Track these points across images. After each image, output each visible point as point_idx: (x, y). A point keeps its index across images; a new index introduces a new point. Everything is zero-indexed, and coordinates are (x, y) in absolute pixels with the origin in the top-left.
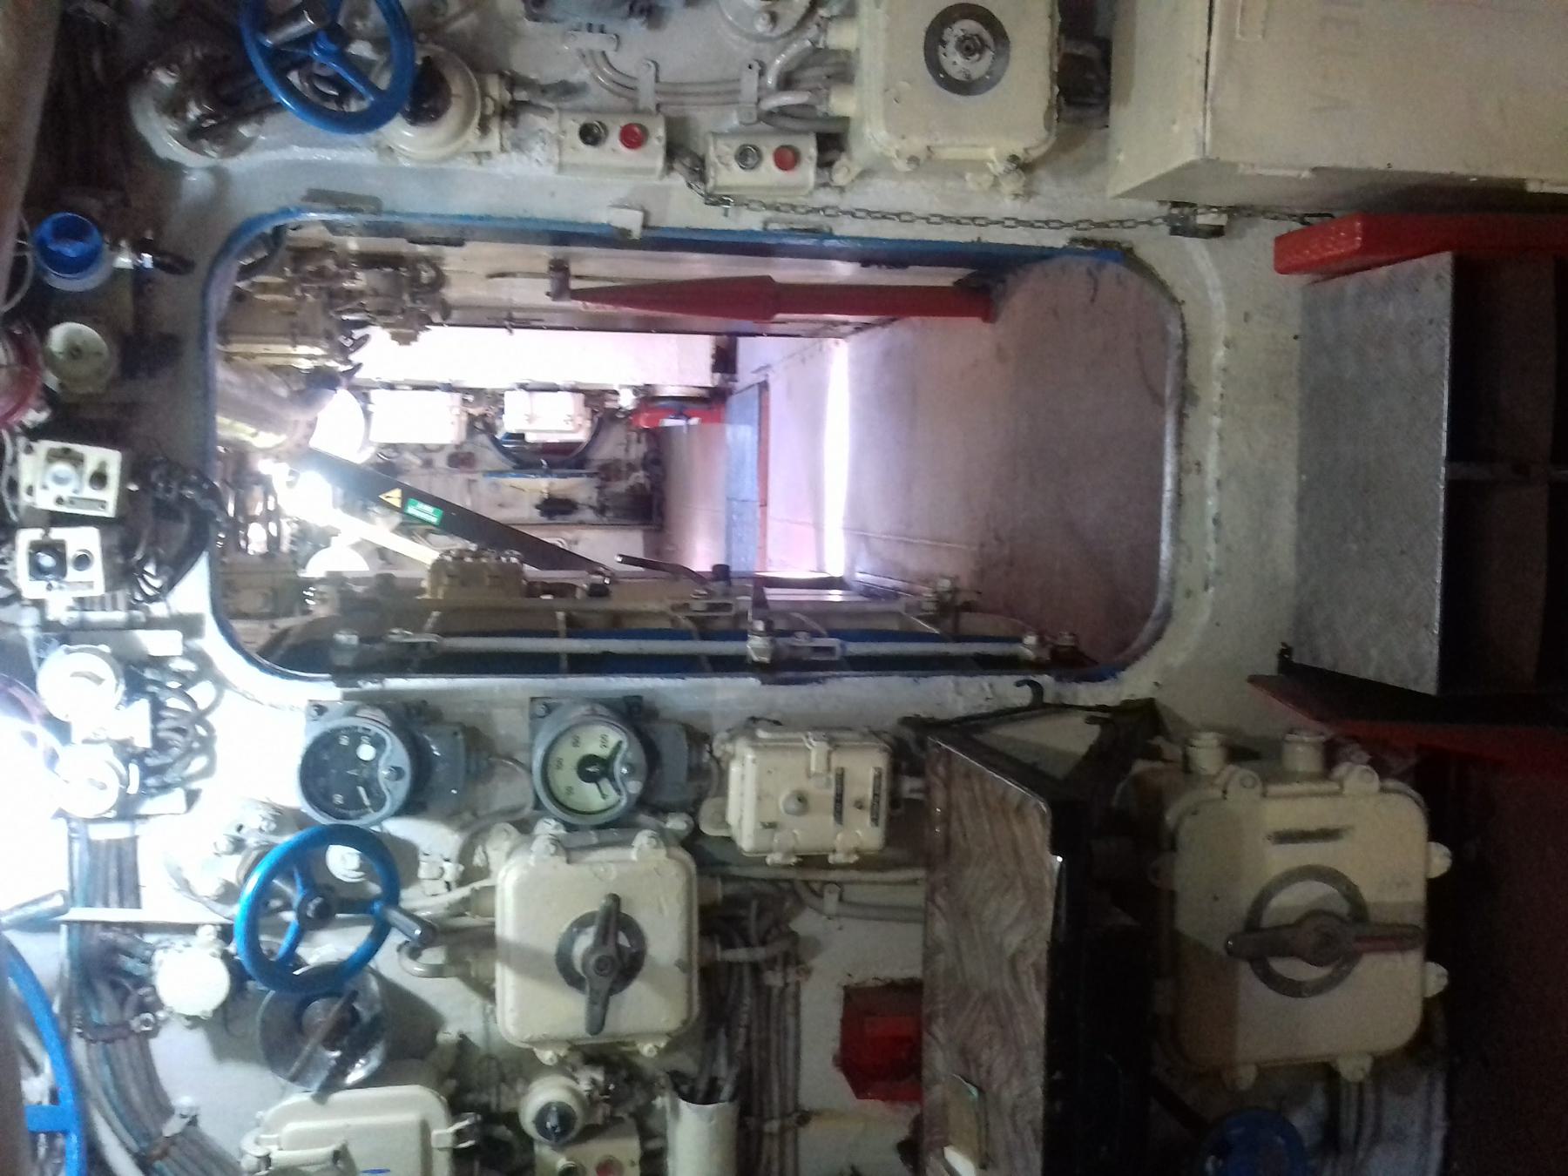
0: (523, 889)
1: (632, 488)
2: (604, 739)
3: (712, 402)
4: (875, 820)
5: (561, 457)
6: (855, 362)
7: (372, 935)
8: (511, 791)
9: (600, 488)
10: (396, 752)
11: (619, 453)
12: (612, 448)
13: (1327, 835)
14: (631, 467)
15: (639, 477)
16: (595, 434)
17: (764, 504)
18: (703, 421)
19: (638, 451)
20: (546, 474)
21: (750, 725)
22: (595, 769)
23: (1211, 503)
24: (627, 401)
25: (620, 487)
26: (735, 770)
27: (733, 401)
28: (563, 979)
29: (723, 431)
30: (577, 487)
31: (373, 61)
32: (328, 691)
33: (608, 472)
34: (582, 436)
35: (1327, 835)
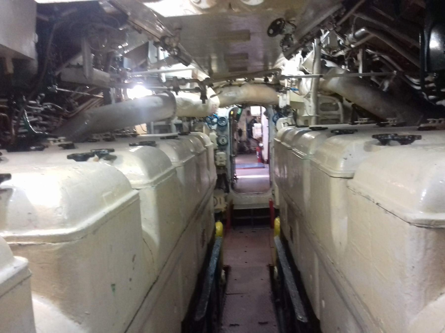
0: (213, 135)
1: (245, 147)
2: (225, 141)
3: (261, 160)
4: (220, 165)
5: (250, 133)
6: (267, 178)
7: (210, 124)
8: (220, 133)
9: (244, 141)
10: (224, 124)
11: (252, 145)
12: (253, 143)
13: (220, 203)
14: (249, 147)
15: (247, 149)
16: (255, 139)
17: (244, 169)
18: (258, 159)
19: (252, 148)
20: (247, 131)
21: (227, 154)
22: (223, 140)
23: (248, 197)
24: (261, 145)
25: (245, 145)
26: (223, 152)
27: (262, 164)
28: (444, 105)
29: (257, 162)
30: (245, 136)
31: (374, 54)
32: (228, 117)
33: (248, 143)
34: (254, 137)
35: (220, 203)
